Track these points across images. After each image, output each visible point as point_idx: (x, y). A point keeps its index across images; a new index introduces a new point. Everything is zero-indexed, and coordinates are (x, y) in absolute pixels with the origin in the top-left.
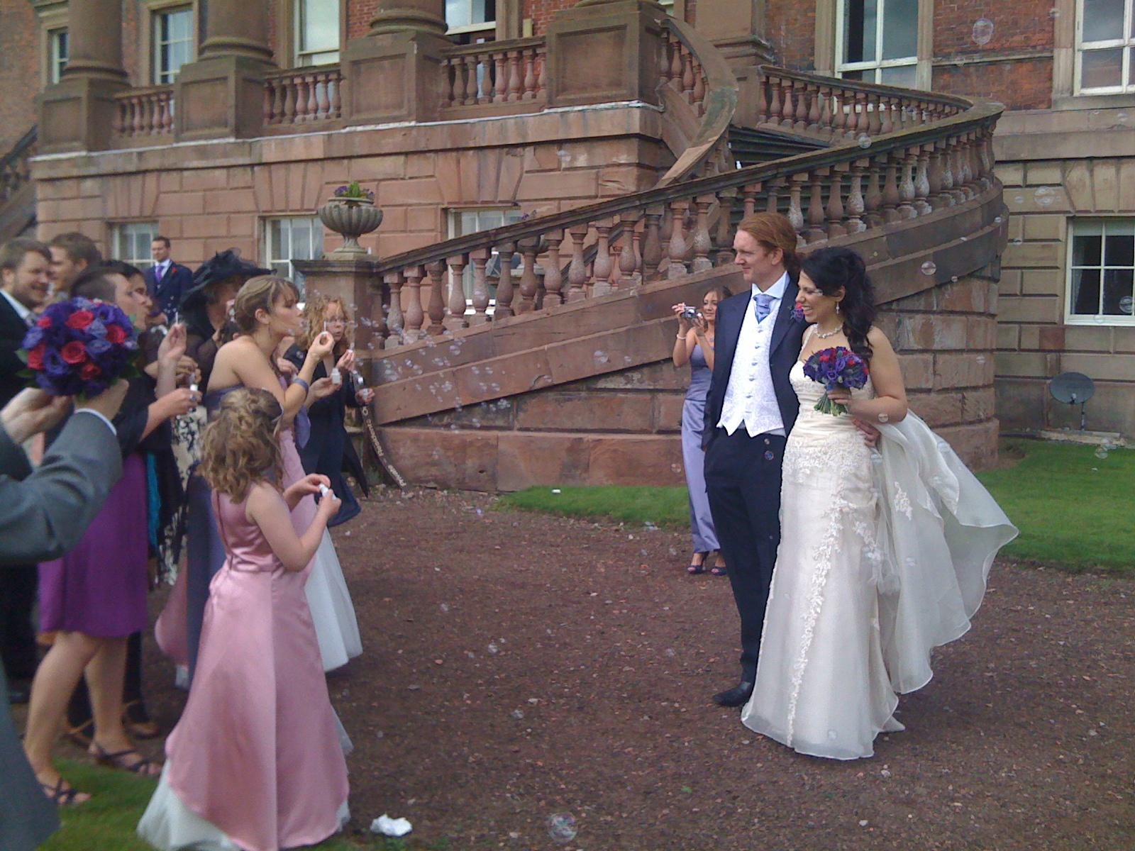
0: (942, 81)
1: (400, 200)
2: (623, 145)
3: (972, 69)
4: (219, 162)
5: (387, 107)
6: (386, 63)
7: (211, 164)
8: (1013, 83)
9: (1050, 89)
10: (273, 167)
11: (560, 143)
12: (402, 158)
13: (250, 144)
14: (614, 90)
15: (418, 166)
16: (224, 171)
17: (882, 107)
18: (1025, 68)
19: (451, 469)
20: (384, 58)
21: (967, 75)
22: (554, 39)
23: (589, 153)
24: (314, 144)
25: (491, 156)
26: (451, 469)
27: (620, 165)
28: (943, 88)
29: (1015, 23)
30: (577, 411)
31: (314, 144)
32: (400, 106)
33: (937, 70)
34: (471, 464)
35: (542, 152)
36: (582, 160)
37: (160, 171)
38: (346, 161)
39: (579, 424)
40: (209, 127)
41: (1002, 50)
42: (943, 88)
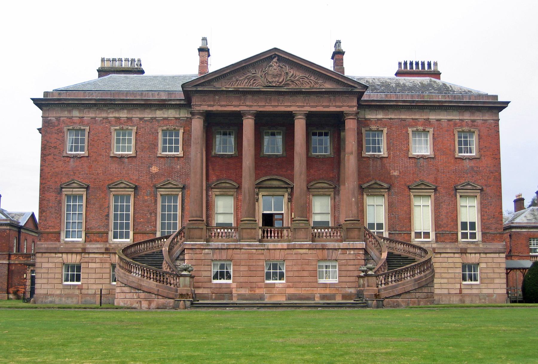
0: (390, 236)
1: (307, 259)
2: (361, 250)
3: (396, 234)
4: (254, 248)
5: (303, 239)
6: (303, 230)
7: (252, 248)
8: (404, 237)
9: (411, 239)
10: (270, 250)
11: (347, 249)
12: (308, 250)
13: (265, 244)
14: (359, 239)
15: (311, 251)
16: (255, 250)
17: (405, 246)
18: (406, 234)
19: (392, 305)
20: (303, 228)
21: (395, 235)
22: (345, 229)
23: (354, 251)
24: (285, 245)
25: (331, 251)
26: (392, 305)
27: (360, 254)
28: (391, 237)
29: (403, 226)
30: (407, 296)
31: (285, 245)
32: (307, 239)
33: (389, 234)
34: (395, 304)
35: (343, 251)
36: (352, 252)
37: (233, 249)
38: (292, 250)
39: (408, 297)
40: (249, 239)
41: (401, 231)
42: (391, 237)
